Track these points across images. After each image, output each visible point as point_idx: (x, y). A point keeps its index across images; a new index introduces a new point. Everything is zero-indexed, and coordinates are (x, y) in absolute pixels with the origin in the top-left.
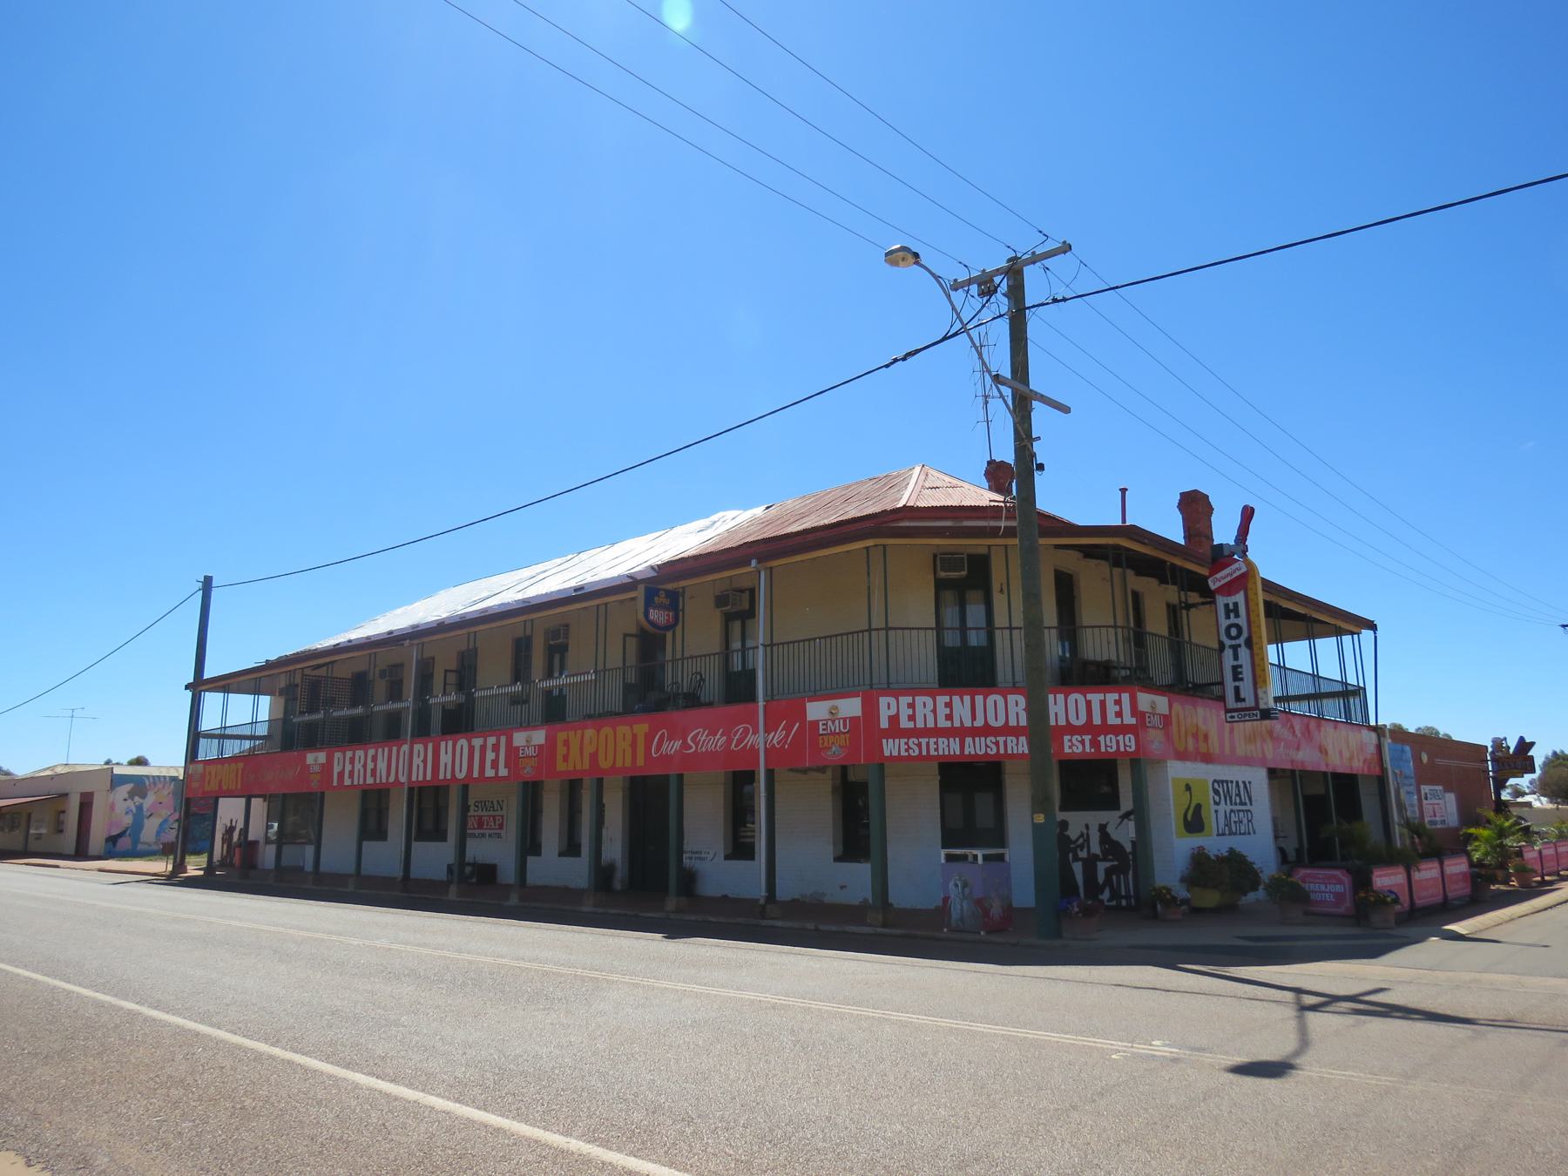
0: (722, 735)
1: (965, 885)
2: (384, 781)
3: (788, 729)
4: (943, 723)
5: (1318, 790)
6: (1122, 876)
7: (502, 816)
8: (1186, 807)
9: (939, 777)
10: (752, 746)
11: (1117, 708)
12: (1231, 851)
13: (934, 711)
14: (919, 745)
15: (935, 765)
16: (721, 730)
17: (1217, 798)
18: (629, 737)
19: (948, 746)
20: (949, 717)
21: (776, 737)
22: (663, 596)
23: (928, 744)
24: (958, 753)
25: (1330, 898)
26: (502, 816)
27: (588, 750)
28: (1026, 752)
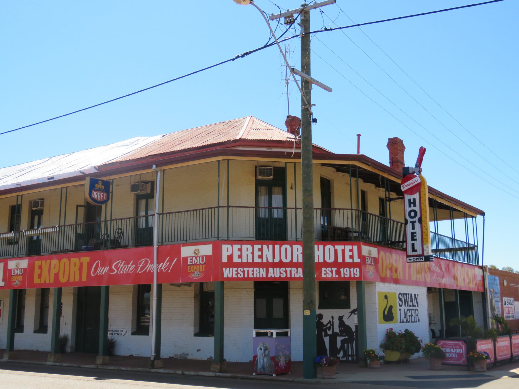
0: (132, 264)
1: (266, 349)
3: (171, 261)
4: (257, 260)
5: (452, 299)
6: (350, 344)
9: (254, 290)
10: (150, 271)
11: (351, 254)
13: (253, 253)
17: (401, 303)
19: (260, 272)
21: (163, 266)
22: (101, 184)
24: (265, 276)
27: (54, 271)
28: (302, 276)
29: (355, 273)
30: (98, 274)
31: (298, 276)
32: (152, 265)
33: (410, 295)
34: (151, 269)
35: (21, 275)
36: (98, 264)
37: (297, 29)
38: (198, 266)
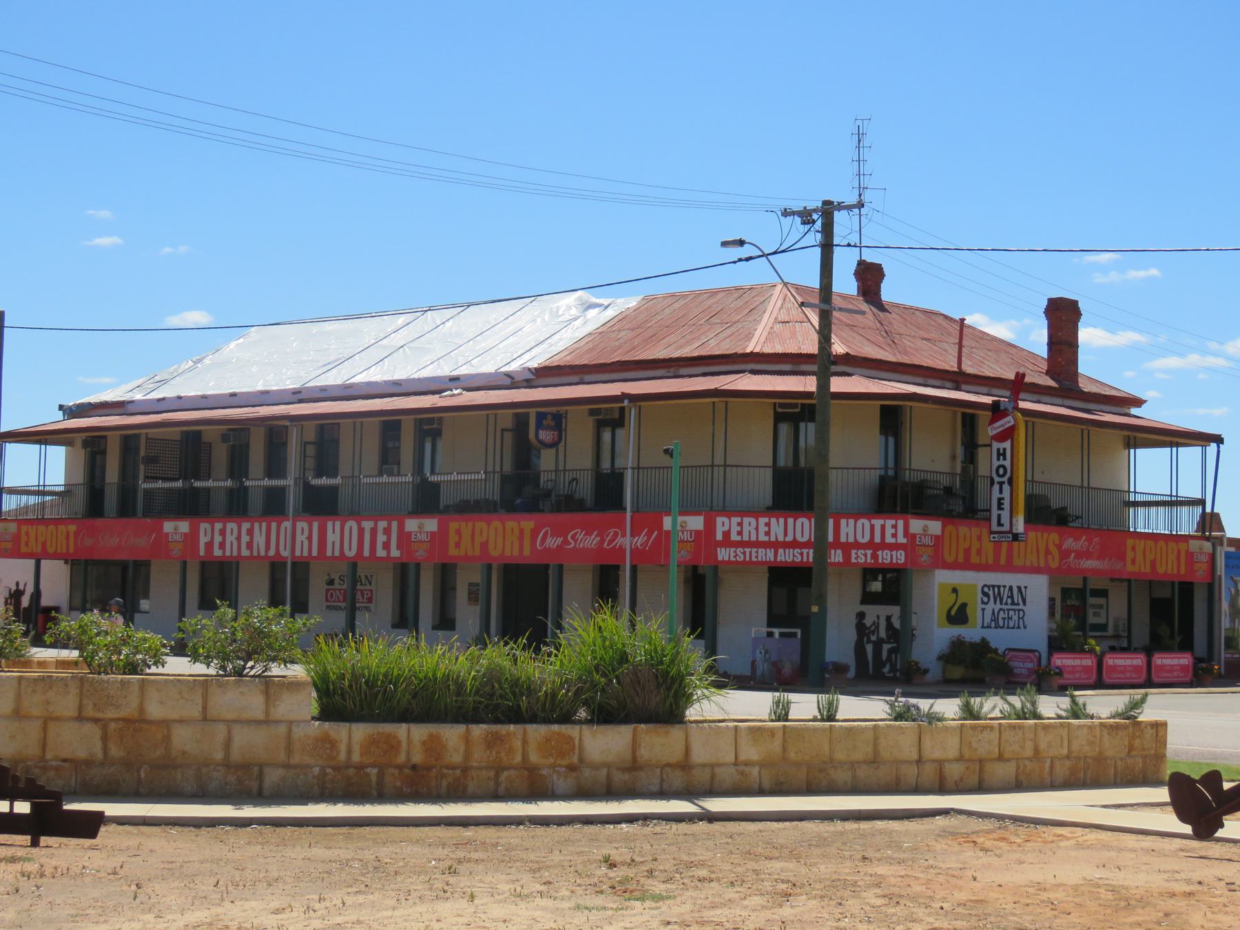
0: (596, 536)
1: (766, 652)
3: (649, 535)
4: (763, 538)
5: (1166, 594)
7: (371, 591)
8: (951, 604)
9: (768, 575)
10: (621, 546)
11: (893, 531)
12: (983, 639)
13: (757, 529)
15: (765, 569)
16: (596, 532)
17: (985, 599)
18: (517, 532)
19: (766, 555)
20: (768, 533)
21: (640, 541)
23: (751, 552)
24: (772, 559)
25: (1025, 672)
26: (371, 591)
29: (899, 557)
33: (1007, 589)
35: (690, 542)
36: (546, 533)
37: (815, 238)
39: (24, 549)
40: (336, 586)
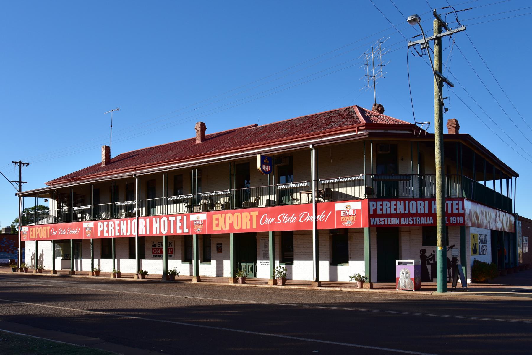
0: (294, 216)
1: (407, 273)
2: (125, 234)
3: (326, 214)
4: (393, 212)
6: (448, 270)
7: (172, 249)
9: (376, 233)
10: (309, 221)
13: (390, 207)
14: (384, 220)
16: (294, 214)
18: (249, 218)
19: (395, 221)
22: (267, 159)
23: (387, 220)
24: (398, 223)
26: (172, 249)
27: (37, 233)
28: (432, 223)
29: (453, 220)
30: (288, 222)
31: (421, 223)
32: (269, 219)
34: (310, 220)
38: (349, 217)
39: (31, 237)
40: (157, 247)
